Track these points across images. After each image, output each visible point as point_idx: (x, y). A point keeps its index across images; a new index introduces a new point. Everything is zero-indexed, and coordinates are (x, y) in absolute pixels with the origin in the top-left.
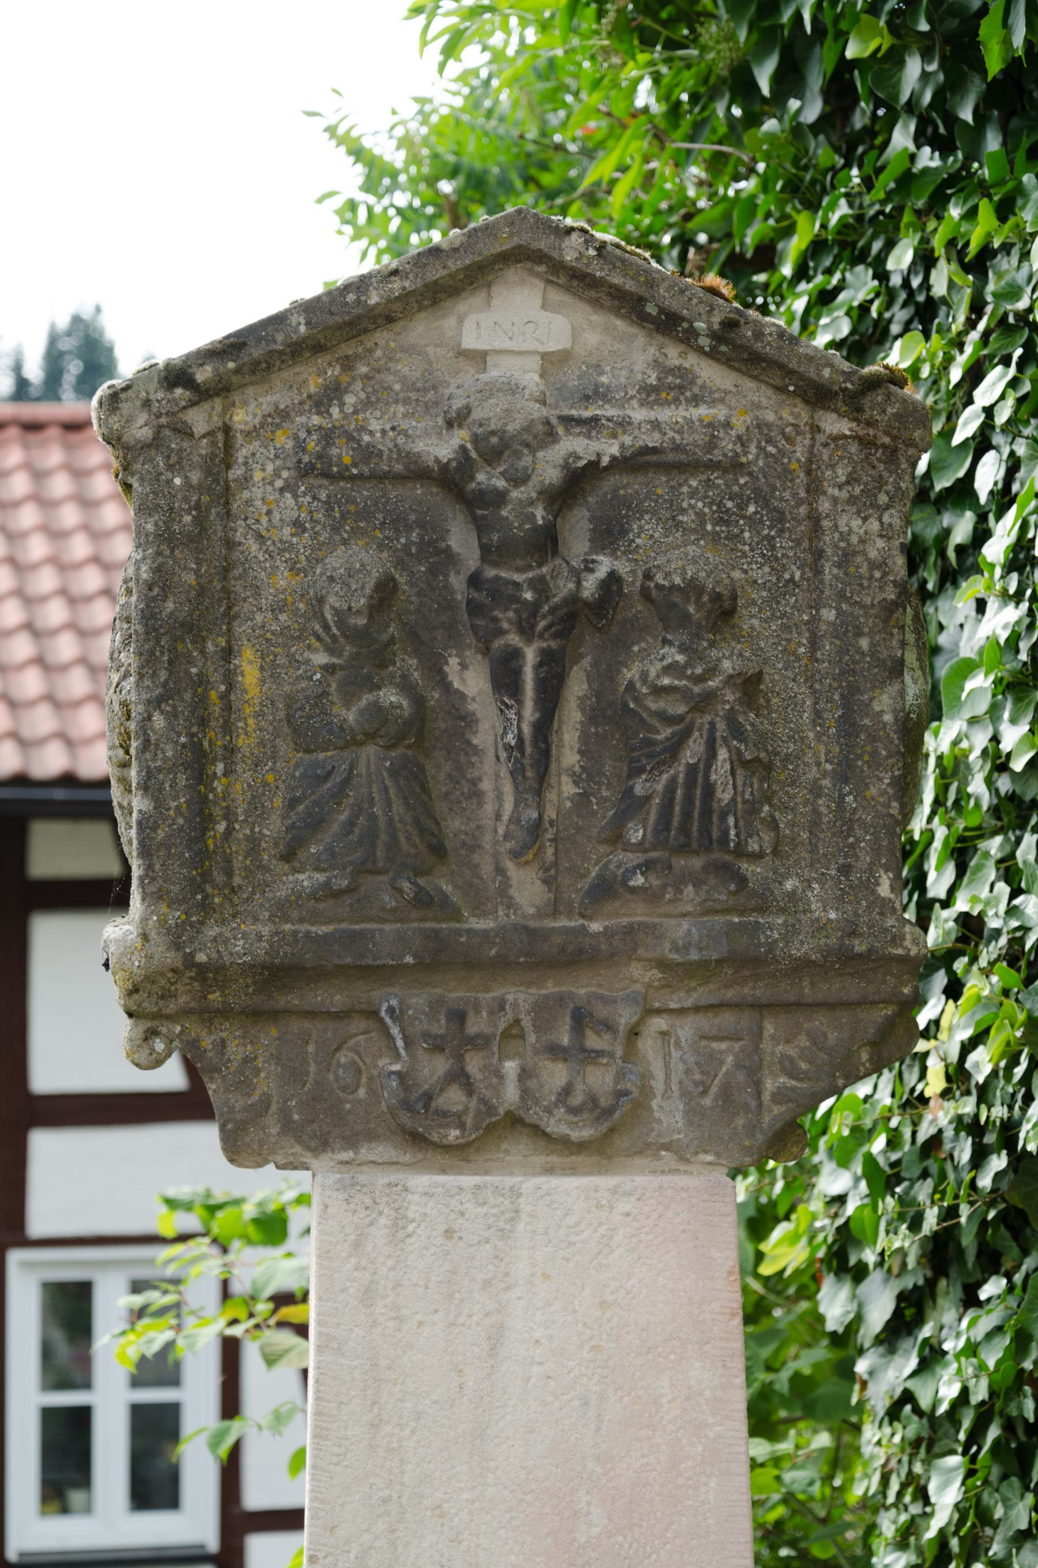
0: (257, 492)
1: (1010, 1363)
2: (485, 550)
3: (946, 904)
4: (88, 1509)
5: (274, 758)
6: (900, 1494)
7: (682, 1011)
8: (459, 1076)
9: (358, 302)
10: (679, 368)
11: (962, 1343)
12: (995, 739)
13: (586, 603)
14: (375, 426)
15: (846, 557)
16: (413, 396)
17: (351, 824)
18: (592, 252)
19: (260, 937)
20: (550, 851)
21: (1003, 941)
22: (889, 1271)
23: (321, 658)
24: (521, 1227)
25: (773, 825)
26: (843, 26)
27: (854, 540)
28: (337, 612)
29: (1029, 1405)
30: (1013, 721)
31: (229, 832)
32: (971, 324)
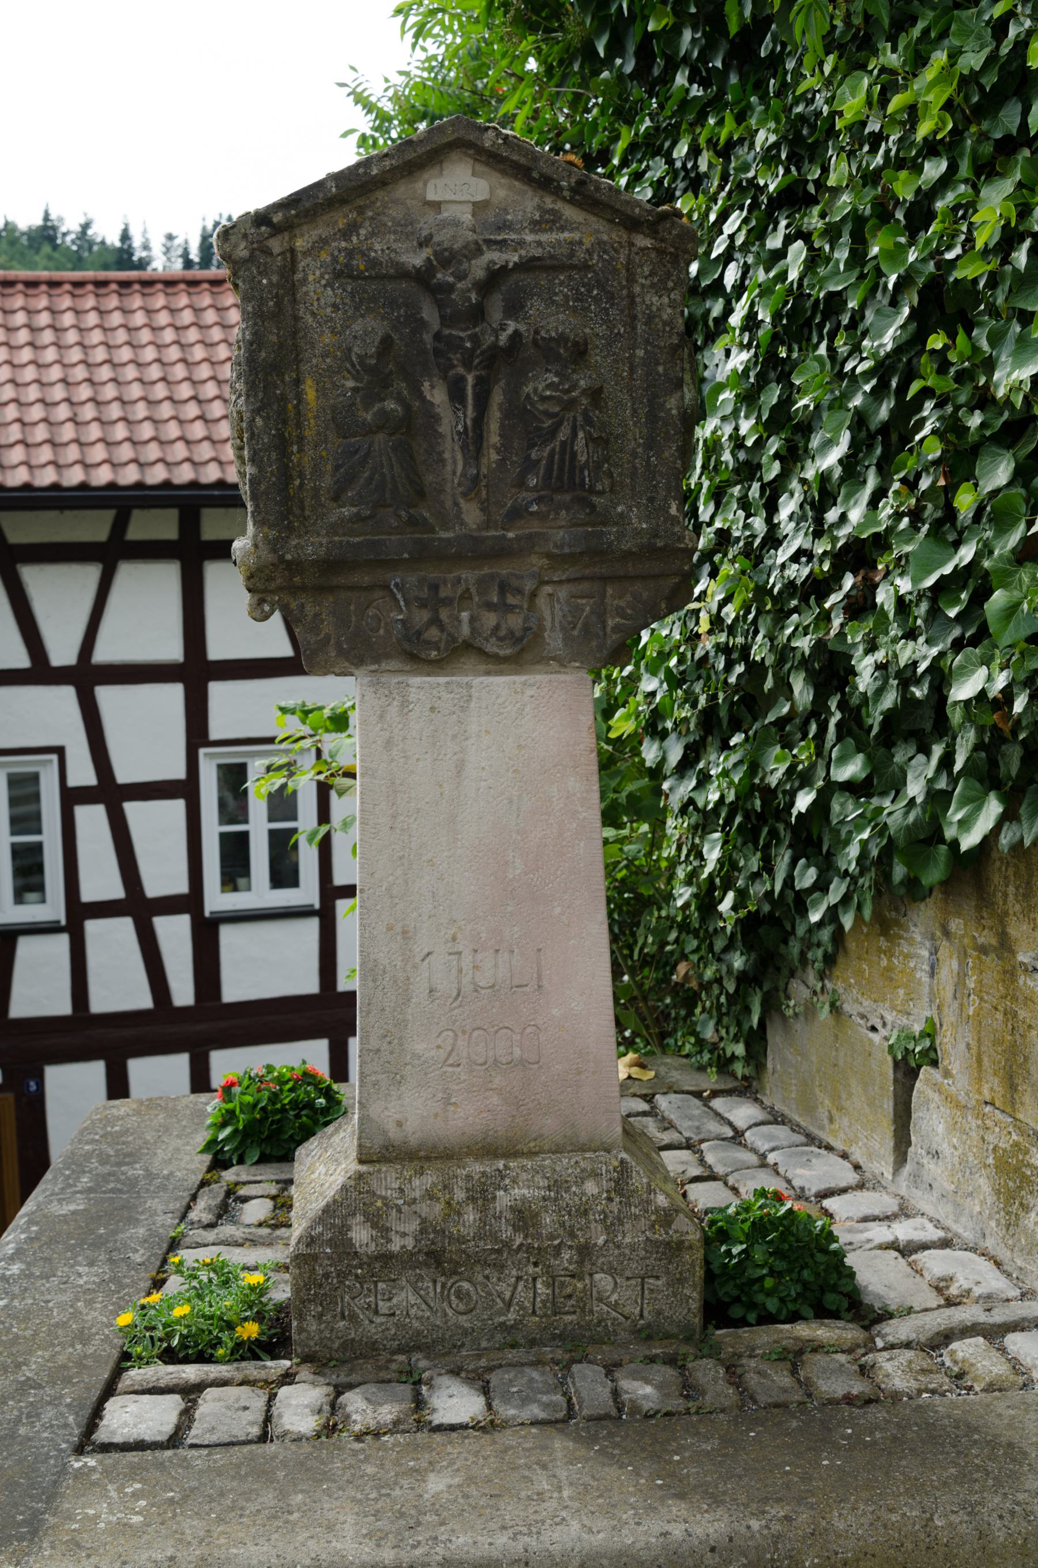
0: (311, 287)
1: (746, 780)
2: (442, 318)
3: (710, 524)
4: (249, 888)
5: (326, 442)
6: (688, 856)
7: (560, 582)
8: (435, 621)
9: (365, 173)
10: (552, 210)
11: (720, 769)
12: (737, 429)
13: (501, 348)
14: (377, 247)
15: (650, 319)
16: (399, 229)
17: (371, 479)
18: (500, 141)
19: (321, 545)
20: (484, 492)
21: (741, 544)
22: (680, 733)
23: (350, 384)
24: (472, 705)
25: (610, 475)
26: (646, 12)
27: (654, 309)
28: (359, 356)
29: (758, 803)
30: (747, 417)
31: (302, 485)
32: (721, 188)
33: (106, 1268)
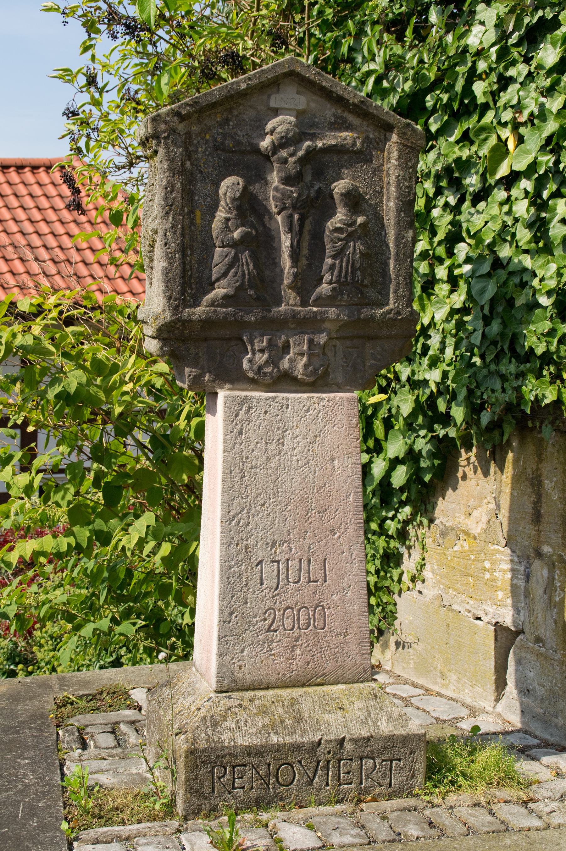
33: (18, 369)
